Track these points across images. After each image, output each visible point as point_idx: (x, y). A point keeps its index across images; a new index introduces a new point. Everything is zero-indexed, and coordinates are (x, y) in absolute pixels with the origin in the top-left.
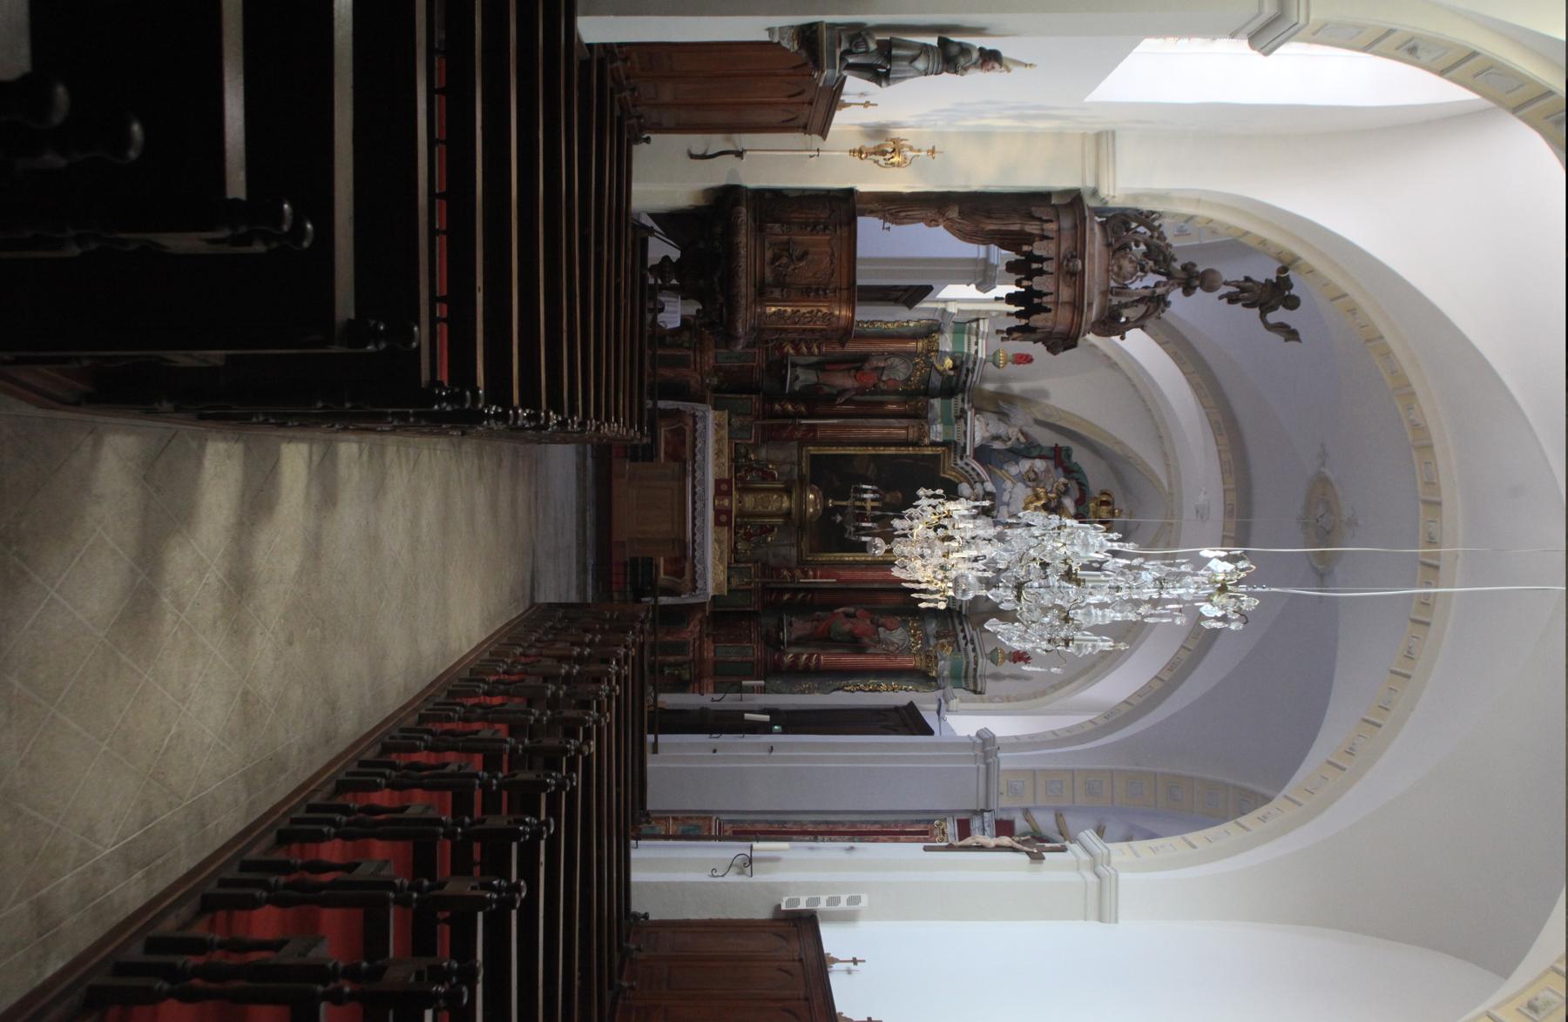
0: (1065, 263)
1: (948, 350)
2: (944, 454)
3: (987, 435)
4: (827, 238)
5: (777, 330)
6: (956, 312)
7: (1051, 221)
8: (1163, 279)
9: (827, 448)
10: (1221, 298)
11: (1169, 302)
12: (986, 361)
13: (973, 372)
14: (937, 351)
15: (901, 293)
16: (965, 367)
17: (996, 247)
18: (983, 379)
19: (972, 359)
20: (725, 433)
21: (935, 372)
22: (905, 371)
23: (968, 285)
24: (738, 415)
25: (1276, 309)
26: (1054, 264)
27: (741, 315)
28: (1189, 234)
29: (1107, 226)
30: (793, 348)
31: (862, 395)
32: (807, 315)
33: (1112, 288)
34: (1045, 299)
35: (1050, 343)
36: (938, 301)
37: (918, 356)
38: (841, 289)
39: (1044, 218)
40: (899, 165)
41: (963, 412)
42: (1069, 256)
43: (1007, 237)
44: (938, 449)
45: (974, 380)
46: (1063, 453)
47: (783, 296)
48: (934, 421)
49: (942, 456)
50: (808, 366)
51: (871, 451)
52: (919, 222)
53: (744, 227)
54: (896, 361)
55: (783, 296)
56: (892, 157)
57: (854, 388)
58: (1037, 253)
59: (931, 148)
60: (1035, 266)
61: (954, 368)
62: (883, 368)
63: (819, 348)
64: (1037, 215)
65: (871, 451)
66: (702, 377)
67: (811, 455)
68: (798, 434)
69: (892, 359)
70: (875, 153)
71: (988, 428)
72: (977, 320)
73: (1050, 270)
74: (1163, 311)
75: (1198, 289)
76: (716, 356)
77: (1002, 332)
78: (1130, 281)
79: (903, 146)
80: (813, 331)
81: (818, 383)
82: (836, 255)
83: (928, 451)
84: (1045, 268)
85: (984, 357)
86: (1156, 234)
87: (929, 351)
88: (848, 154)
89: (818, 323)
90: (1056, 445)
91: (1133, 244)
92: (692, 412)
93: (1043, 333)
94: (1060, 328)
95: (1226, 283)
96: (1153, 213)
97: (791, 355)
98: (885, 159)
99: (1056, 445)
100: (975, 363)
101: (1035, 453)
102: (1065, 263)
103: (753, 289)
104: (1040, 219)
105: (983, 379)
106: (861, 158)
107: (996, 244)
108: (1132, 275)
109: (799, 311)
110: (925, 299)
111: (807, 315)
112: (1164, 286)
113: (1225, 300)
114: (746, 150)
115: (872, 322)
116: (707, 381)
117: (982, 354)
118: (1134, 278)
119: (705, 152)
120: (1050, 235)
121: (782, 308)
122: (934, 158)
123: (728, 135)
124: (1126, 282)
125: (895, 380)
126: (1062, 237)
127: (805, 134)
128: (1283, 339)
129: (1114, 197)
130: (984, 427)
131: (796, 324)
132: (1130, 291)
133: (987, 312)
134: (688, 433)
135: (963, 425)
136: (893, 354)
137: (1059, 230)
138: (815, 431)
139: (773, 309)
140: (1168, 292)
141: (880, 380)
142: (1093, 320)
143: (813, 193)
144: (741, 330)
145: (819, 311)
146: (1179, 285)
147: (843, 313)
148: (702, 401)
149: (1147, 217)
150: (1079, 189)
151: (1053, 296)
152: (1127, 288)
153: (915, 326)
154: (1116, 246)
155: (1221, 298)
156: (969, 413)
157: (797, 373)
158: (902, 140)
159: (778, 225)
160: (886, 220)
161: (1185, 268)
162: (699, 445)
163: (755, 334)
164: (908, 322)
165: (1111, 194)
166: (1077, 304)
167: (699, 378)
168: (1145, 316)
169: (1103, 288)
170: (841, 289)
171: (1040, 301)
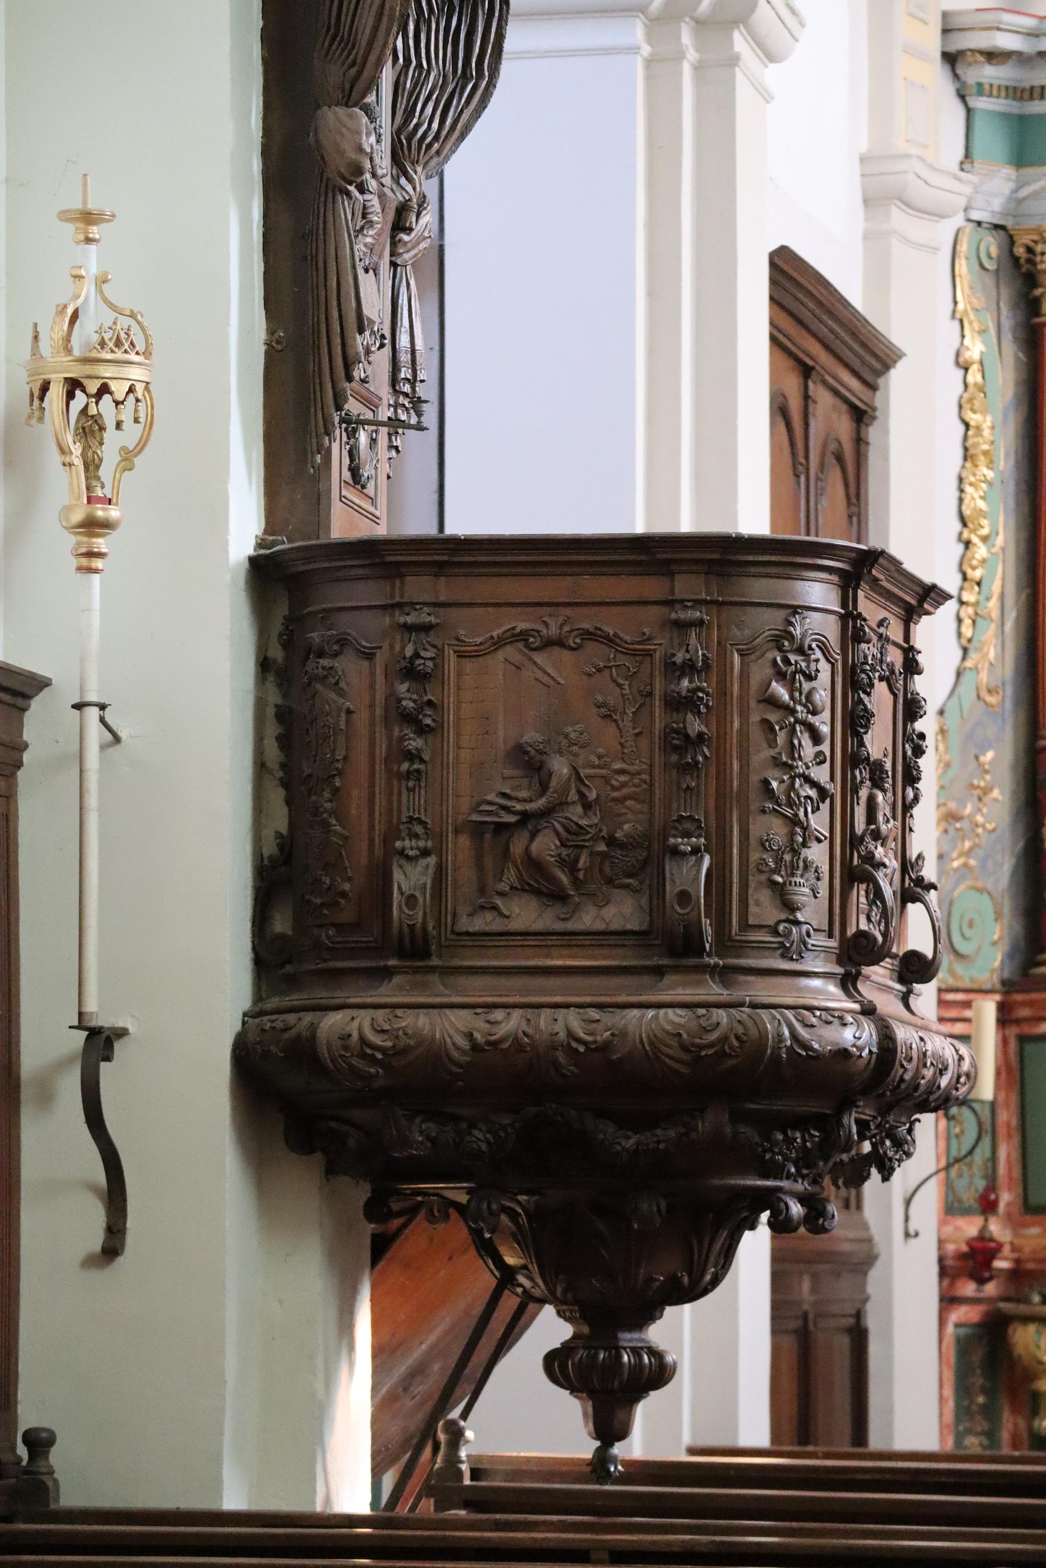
15: (823, 398)
53: (408, 1020)
70: (92, 466)
98: (119, 425)
103: (669, 979)
119: (95, 1189)
123: (26, 1094)
127: (19, 765)
143: (273, 730)
159: (397, 876)
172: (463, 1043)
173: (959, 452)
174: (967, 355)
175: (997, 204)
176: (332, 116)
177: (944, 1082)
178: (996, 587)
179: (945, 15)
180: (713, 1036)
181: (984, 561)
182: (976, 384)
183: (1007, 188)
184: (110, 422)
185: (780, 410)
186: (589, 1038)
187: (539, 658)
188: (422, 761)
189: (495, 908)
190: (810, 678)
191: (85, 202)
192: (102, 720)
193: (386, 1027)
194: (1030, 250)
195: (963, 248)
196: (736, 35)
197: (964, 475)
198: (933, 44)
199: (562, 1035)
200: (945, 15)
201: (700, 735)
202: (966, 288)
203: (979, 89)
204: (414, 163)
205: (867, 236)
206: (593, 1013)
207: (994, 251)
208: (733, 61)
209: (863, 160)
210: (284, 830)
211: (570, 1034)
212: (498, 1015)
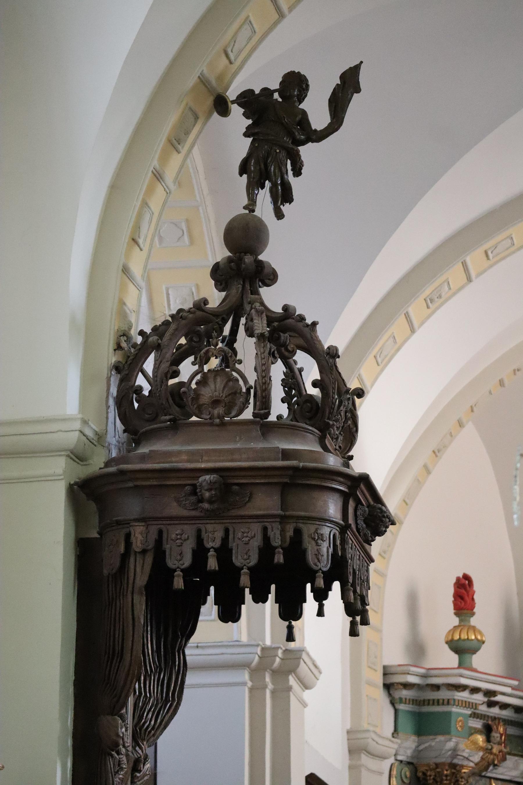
0: (206, 506)
7: (128, 536)
10: (279, 215)
11: (286, 308)
13: (494, 693)
16: (483, 709)
25: (304, 113)
26: (210, 527)
33: (255, 415)
34: (276, 542)
39: (122, 549)
42: (193, 499)
45: (508, 690)
58: (187, 561)
60: (212, 564)
73: (219, 534)
77: (353, 624)
78: (241, 382)
84: (217, 544)
91: (171, 382)
95: (251, 207)
96: (119, 347)
104: (125, 557)
108: (231, 379)
112: (252, 320)
113: (286, 208)
120: (153, 536)
124: (244, 390)
128: (355, 95)
129: (85, 422)
154: (176, 410)
155: (279, 215)
165: (77, 425)
169: (257, 431)
175: (409, 752)
176: (106, 720)
179: (385, 667)
183: (414, 746)
194: (424, 774)
195: (394, 772)
198: (379, 680)
200: (385, 667)
203: (401, 700)
204: (143, 740)
205: (351, 768)
207: (408, 774)
208: (289, 689)
209: (348, 732)
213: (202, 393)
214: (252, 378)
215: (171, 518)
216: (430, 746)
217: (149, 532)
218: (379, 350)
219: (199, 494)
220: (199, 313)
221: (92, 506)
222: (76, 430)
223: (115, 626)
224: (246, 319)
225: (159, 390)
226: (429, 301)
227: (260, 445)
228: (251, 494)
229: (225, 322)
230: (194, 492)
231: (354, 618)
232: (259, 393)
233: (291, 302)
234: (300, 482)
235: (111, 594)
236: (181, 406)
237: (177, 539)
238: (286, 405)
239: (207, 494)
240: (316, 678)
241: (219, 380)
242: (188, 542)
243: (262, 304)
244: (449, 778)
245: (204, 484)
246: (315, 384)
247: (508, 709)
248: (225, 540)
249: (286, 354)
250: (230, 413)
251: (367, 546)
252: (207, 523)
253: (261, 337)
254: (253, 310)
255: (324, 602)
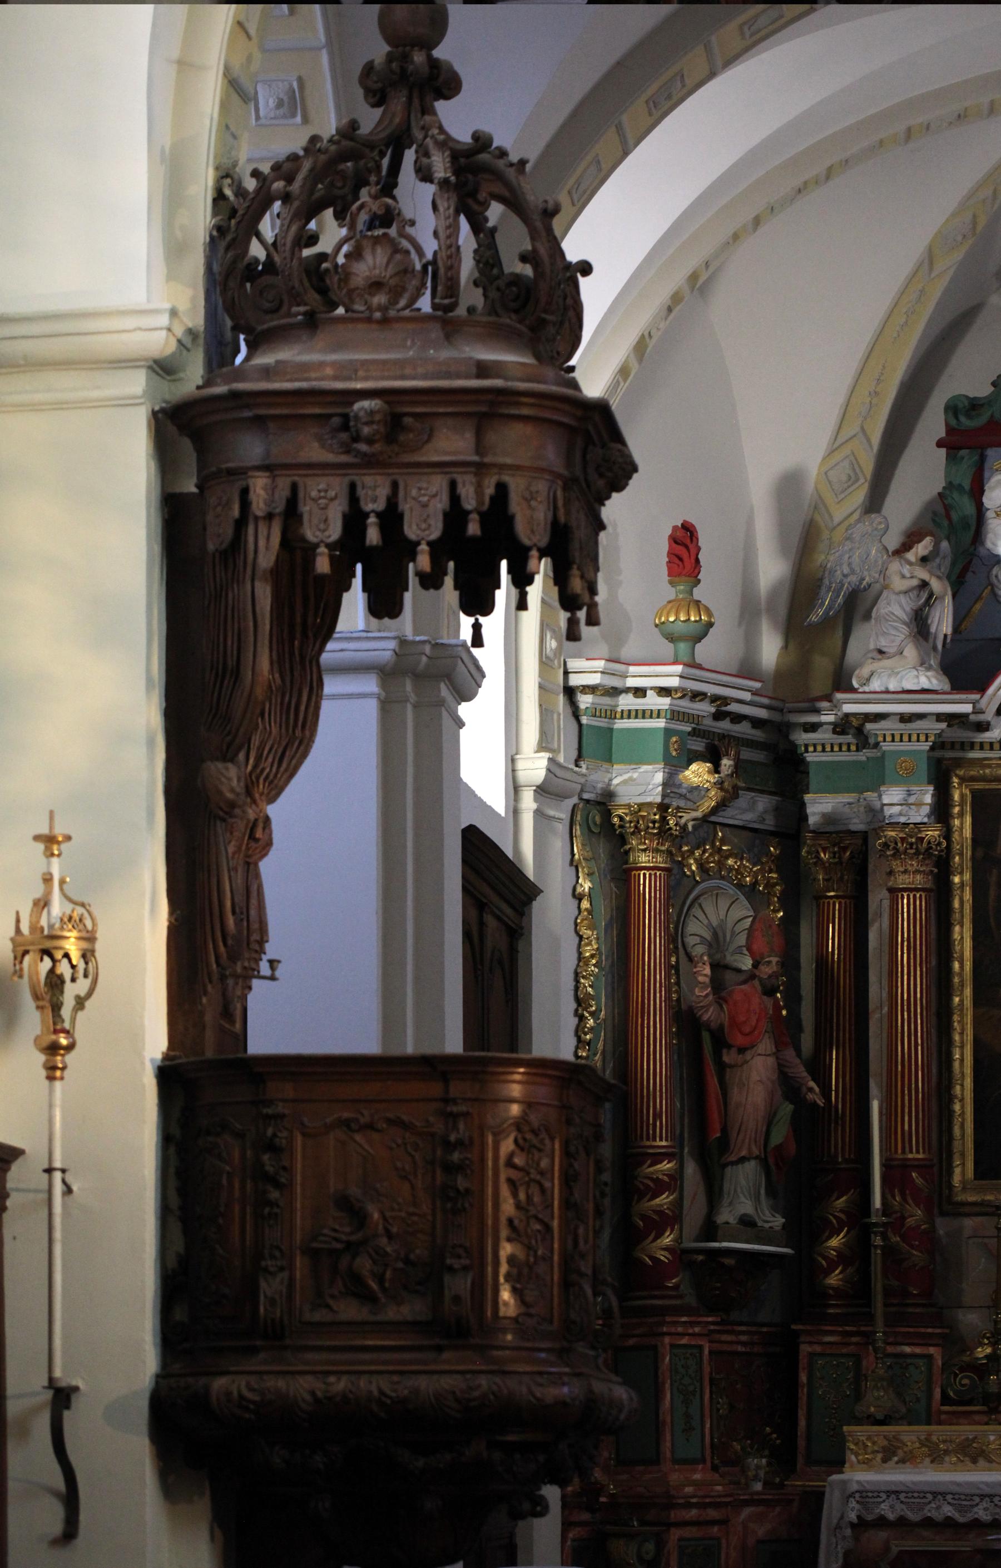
0: (363, 447)
1: (659, 777)
2: (973, 779)
3: (911, 652)
4: (299, 1139)
5: (566, 1284)
6: (546, 755)
7: (245, 492)
8: (410, 156)
9: (957, 1131)
11: (476, 136)
12: (692, 664)
13: (725, 700)
14: (663, 808)
16: (708, 723)
17: (330, 646)
18: (747, 670)
19: (685, 705)
20: (910, 1435)
21: (730, 812)
22: (723, 904)
23: (461, 724)
24: (858, 1396)
26: (368, 480)
27: (524, 1390)
28: (300, 80)
29: (260, 328)
30: (660, 1235)
31: (800, 1028)
32: (522, 1196)
33: (435, 306)
34: (469, 503)
35: (601, 483)
36: (515, 812)
37: (681, 865)
38: (446, 1101)
39: (236, 512)
40: (89, 938)
41: (843, 725)
42: (344, 436)
43: (299, 620)
44: (956, 797)
45: (747, 696)
46: (966, 422)
47: (465, 1268)
48: (875, 813)
49: (979, 786)
50: (714, 1193)
51: (964, 998)
52: (257, 876)
54: (696, 929)
55: (465, 1268)
56: (67, 956)
57: (776, 1054)
58: (335, 532)
59: (41, 847)
60: (373, 536)
61: (713, 757)
62: (714, 966)
63: (658, 1158)
64: (229, 532)
65: (964, 998)
66: (746, 1503)
67: (979, 1174)
68: (916, 1215)
69: (691, 941)
70: (56, 1007)
71: (892, 650)
72: (570, 692)
73: (383, 492)
74: (503, 153)
75: (437, 53)
76: (685, 1462)
77: (572, 624)
78: (414, 255)
79: (35, 928)
80: (568, 1179)
81: (763, 1161)
82: (346, 1115)
83: (964, 826)
84: (380, 506)
85: (679, 668)
86: (278, 185)
87: (664, 832)
88: (58, 1084)
89: (544, 1163)
90: (940, 444)
91: (306, 252)
92: (848, 1532)
93: (567, 502)
94: (552, 455)
96: (219, 197)
97: (679, 1240)
98: (73, 980)
99: (940, 444)
100: (696, 696)
101: (968, 508)
102: (363, 447)
103: (446, 1355)
104: (240, 524)
105: (747, 670)
106: (70, 1047)
107: (321, 649)
108: (396, 249)
109: (510, 1221)
110: (510, 853)
111: (522, 1196)
112: (427, 155)
114: (51, 1380)
115: (581, 1001)
116: (758, 1487)
117: (671, 676)
118: (405, 244)
119: (56, 1494)
120: (283, 492)
121: (504, 1268)
122: (68, 838)
123: (11, 1430)
124: (418, 267)
125: (751, 930)
126: (289, 460)
129: (174, 313)
130: (886, 663)
131: (548, 1228)
132: (443, 255)
133: (545, 663)
134: (910, 1545)
135: (883, 724)
136: (675, 940)
137: (268, 468)
138: (906, 1166)
139: (506, 1295)
140: (447, 143)
141: (752, 976)
142: (528, 360)
144: (566, 1390)
145: (510, 1164)
146: (427, 110)
147: (516, 1090)
148: (816, 1499)
149: (233, 212)
150: (154, 414)
151: (459, 479)
152: (434, 262)
153: (590, 875)
154: (313, 297)
156: (848, 708)
157: (732, 1221)
158: (18, 930)
159: (263, 1284)
160: (251, 973)
161: (378, 97)
162: (948, 1510)
163: (581, 1348)
164: (579, 898)
165: (164, 320)
166: (484, 409)
167: (747, 1511)
168: (514, 203)
169: (436, 332)
170: (446, 1101)
171: (474, 516)
172: (308, 1397)
173: (576, 955)
174: (579, 890)
177: (622, 1417)
178: (600, 1046)
180: (476, 1394)
181: (592, 1029)
182: (586, 909)
184: (67, 977)
185: (467, 935)
186: (393, 1394)
187: (358, 1137)
188: (278, 1206)
189: (328, 1306)
190: (540, 1150)
191: (51, 827)
192: (64, 1181)
193: (256, 1387)
196: (442, 686)
197: (579, 970)
199: (376, 1393)
201: (467, 1191)
202: (580, 845)
206: (395, 1378)
210: (181, 1250)
211: (382, 1393)
212: (332, 1379)
213: (354, 271)
214: (430, 246)
215: (310, 466)
216: (631, 779)
217: (276, 487)
218: (575, 183)
219: (353, 429)
220: (345, 143)
221: (187, 445)
222: (161, 329)
223: (225, 630)
224: (417, 152)
225: (288, 266)
226: (651, 104)
227: (446, 354)
228: (432, 430)
229: (382, 154)
230: (345, 427)
231: (573, 614)
232: (442, 271)
233: (486, 128)
234: (506, 411)
235: (218, 580)
236: (323, 291)
237: (320, 498)
238: (480, 291)
239: (366, 430)
240: (476, 683)
241: (379, 250)
242: (337, 502)
243: (441, 129)
244: (657, 825)
245: (362, 414)
246: (524, 258)
247: (744, 722)
248: (392, 503)
249: (476, 207)
250: (397, 303)
251: (596, 505)
252: (365, 474)
253: (444, 184)
254: (428, 140)
255: (528, 589)
